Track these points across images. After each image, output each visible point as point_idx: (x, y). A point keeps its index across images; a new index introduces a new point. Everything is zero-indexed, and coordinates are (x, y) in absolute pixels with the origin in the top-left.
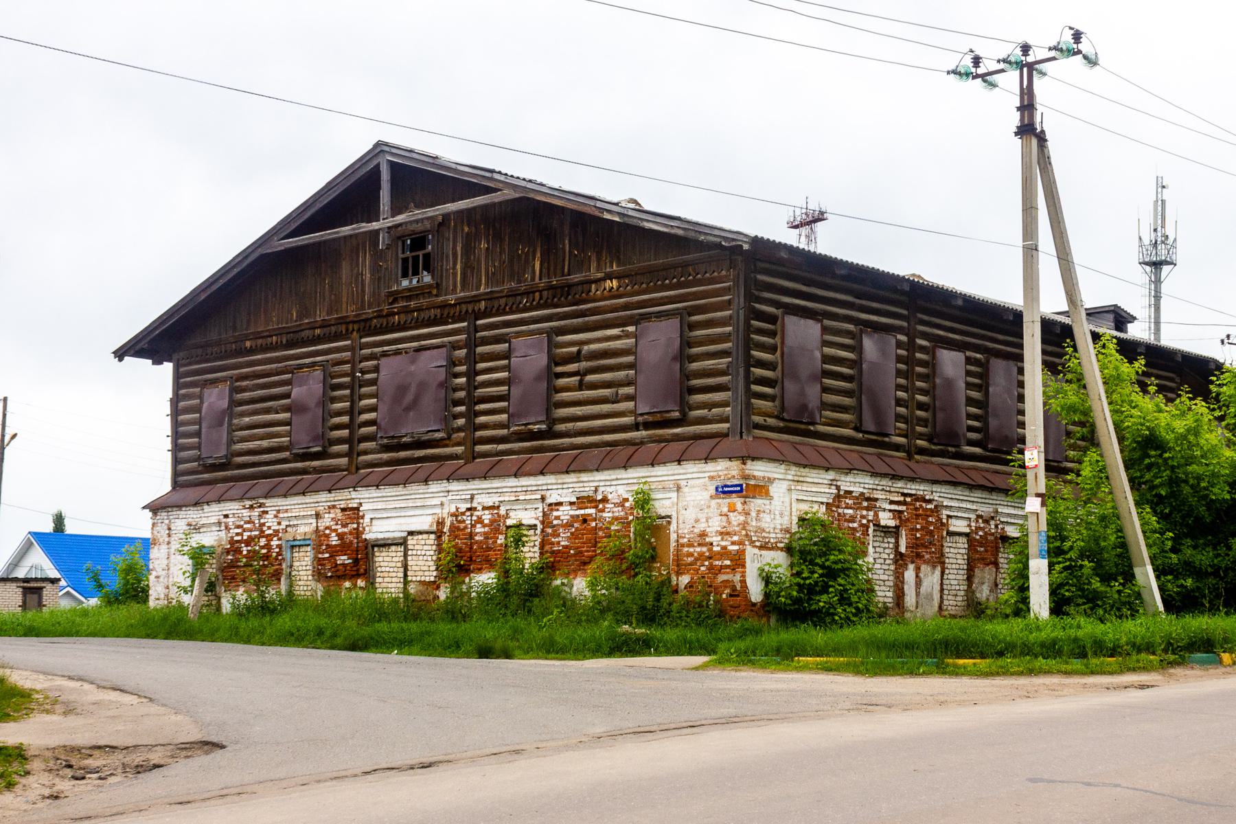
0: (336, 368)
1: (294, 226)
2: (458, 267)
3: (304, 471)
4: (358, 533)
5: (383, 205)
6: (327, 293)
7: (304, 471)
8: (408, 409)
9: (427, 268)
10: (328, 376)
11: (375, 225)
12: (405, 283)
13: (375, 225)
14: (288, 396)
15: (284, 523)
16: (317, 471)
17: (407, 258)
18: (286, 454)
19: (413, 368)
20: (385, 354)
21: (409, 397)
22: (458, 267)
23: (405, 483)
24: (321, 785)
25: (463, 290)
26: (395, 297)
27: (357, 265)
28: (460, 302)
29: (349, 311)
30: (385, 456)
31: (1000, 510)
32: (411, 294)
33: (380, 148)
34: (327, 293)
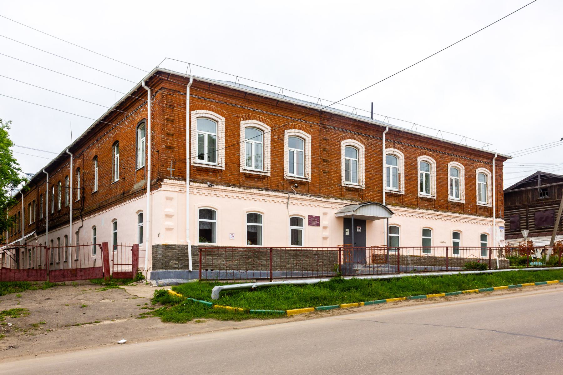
0: (522, 214)
1: (513, 187)
2: (556, 194)
3: (514, 234)
4: (531, 246)
5: (435, 185)
6: (519, 200)
7: (514, 234)
8: (544, 222)
9: (547, 194)
10: (520, 216)
11: (537, 187)
12: (541, 198)
13: (537, 187)
14: (509, 220)
15: (510, 244)
16: (517, 234)
17: (541, 193)
18: (509, 231)
19: (544, 214)
20: (536, 211)
21: (544, 219)
22: (556, 194)
23: (545, 236)
24: (143, 313)
25: (558, 198)
26: (539, 200)
27: (527, 194)
28: (556, 201)
29: (526, 203)
30: (537, 231)
31: (75, 259)
32: (543, 200)
33: (538, 172)
34: (519, 200)
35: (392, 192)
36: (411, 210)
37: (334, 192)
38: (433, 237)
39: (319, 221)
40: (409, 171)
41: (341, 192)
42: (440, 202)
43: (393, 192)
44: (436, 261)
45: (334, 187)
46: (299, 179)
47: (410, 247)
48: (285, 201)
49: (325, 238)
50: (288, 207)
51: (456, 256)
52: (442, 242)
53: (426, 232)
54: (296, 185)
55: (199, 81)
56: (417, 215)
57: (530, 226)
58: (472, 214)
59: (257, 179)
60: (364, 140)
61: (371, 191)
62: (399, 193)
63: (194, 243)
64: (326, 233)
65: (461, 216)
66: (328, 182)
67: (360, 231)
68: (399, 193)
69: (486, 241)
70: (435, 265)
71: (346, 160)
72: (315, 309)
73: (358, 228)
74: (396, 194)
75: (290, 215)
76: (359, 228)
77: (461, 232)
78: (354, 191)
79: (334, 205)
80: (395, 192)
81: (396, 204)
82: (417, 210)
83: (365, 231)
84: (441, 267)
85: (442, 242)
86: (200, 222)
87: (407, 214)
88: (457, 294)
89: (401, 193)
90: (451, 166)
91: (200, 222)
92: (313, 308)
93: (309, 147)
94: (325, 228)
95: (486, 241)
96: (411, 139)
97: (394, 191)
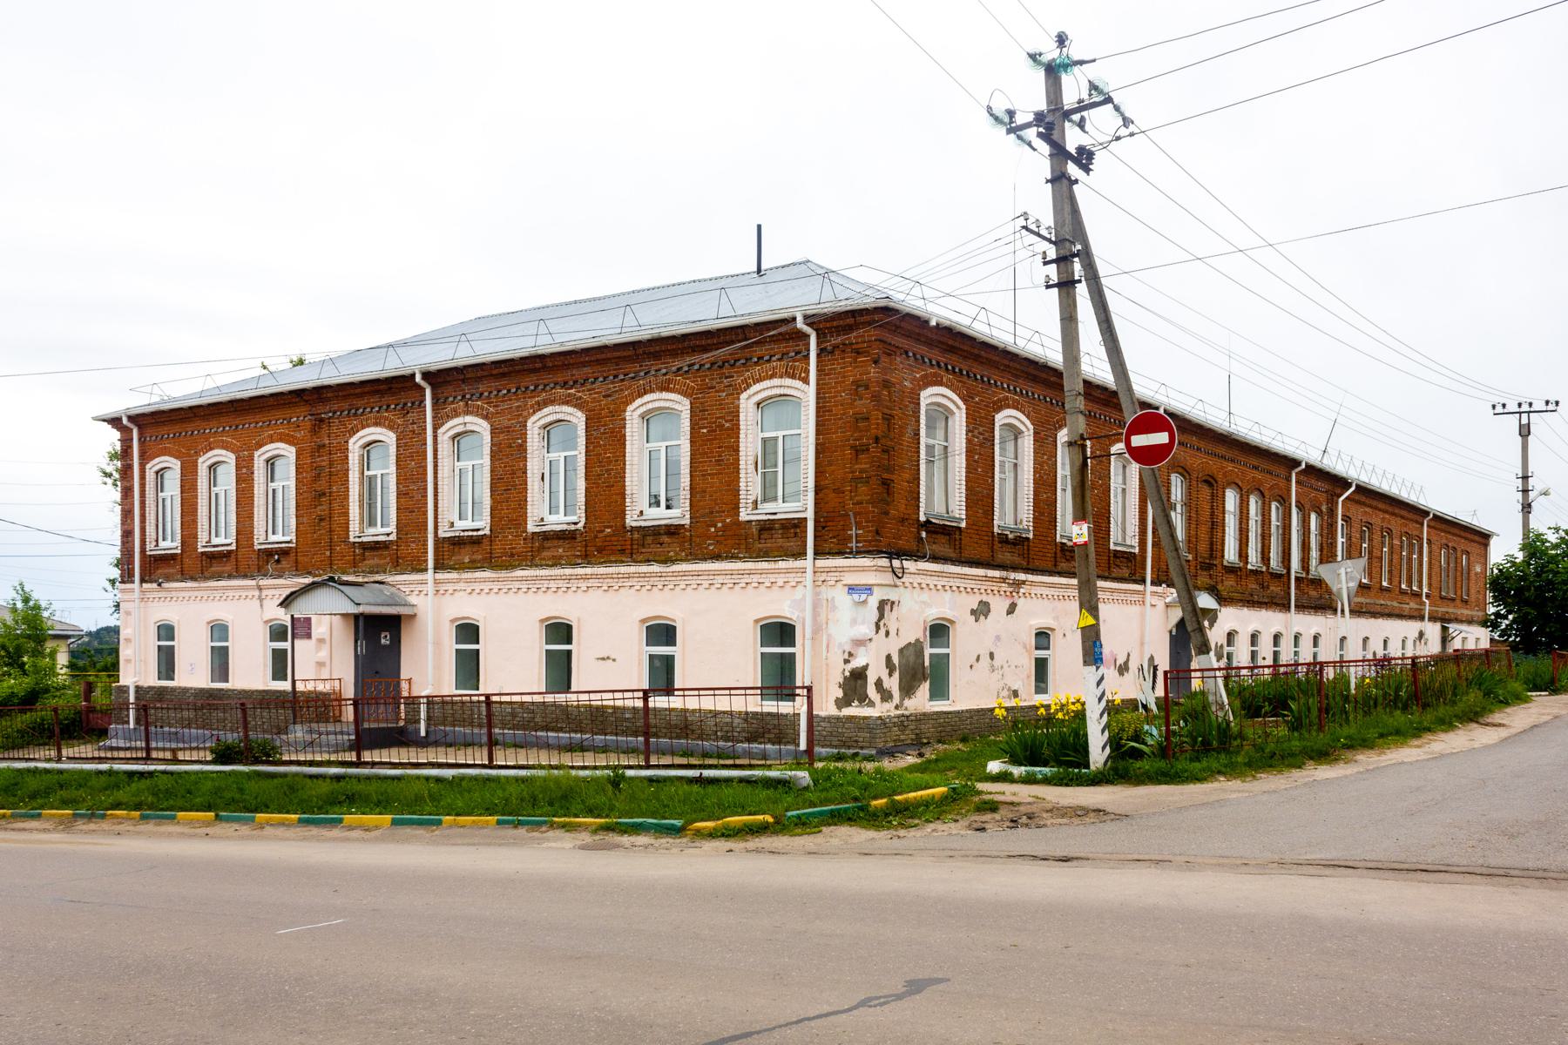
35: (457, 534)
36: (503, 574)
37: (338, 560)
38: (541, 648)
39: (310, 629)
40: (505, 467)
41: (354, 556)
42: (601, 535)
43: (462, 534)
44: (685, 726)
45: (338, 548)
46: (276, 546)
47: (730, 689)
48: (257, 593)
49: (320, 664)
50: (261, 606)
51: (940, 706)
52: (603, 659)
53: (560, 631)
54: (276, 557)
55: (983, 342)
56: (524, 586)
57: (1275, 563)
58: (716, 557)
59: (225, 559)
60: (398, 418)
61: (414, 542)
62: (475, 533)
63: (924, 708)
64: (323, 654)
65: (668, 570)
66: (324, 539)
67: (388, 642)
68: (475, 533)
69: (793, 645)
70: (560, 730)
71: (927, 446)
72: (217, 816)
73: (382, 636)
74: (472, 536)
75: (265, 619)
76: (386, 636)
77: (952, 622)
78: (380, 548)
79: (970, 584)
80: (466, 534)
81: (470, 565)
82: (519, 573)
83: (400, 641)
84: (579, 735)
85: (603, 659)
86: (762, 654)
87: (496, 587)
88: (540, 824)
89: (480, 533)
90: (929, 401)
91: (762, 654)
92: (213, 814)
93: (747, 447)
94: (321, 641)
95: (793, 645)
96: (504, 375)
97: (463, 531)
